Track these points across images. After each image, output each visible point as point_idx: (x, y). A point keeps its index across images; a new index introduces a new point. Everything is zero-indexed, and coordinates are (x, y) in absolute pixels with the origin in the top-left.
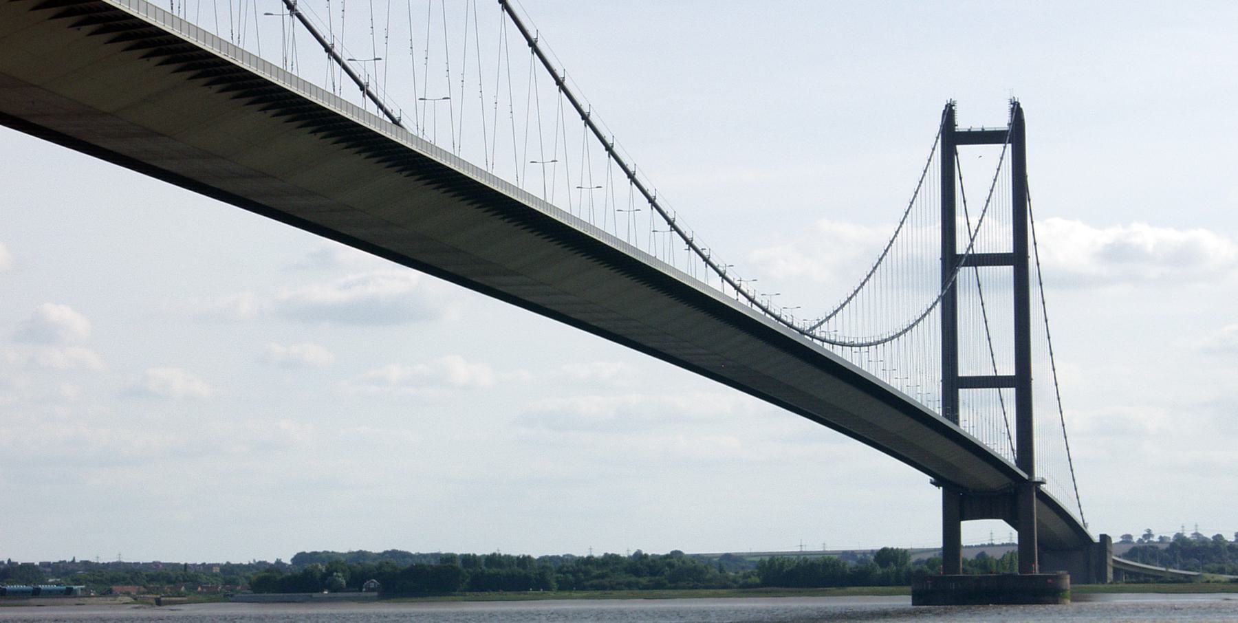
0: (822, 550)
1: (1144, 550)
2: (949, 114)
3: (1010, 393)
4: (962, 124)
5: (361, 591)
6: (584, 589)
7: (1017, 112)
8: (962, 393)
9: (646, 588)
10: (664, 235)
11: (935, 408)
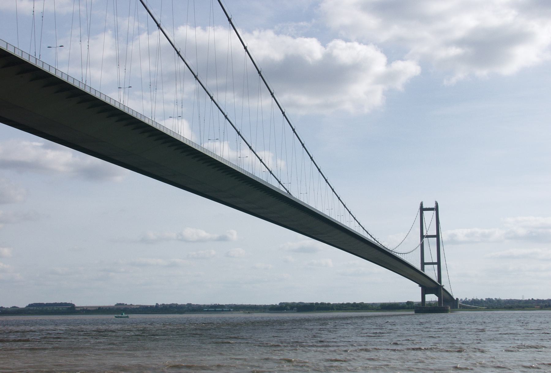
1: (466, 302)
2: (422, 204)
3: (436, 266)
4: (424, 207)
6: (342, 310)
8: (435, 234)
9: (355, 310)
10: (428, 237)
11: (418, 266)
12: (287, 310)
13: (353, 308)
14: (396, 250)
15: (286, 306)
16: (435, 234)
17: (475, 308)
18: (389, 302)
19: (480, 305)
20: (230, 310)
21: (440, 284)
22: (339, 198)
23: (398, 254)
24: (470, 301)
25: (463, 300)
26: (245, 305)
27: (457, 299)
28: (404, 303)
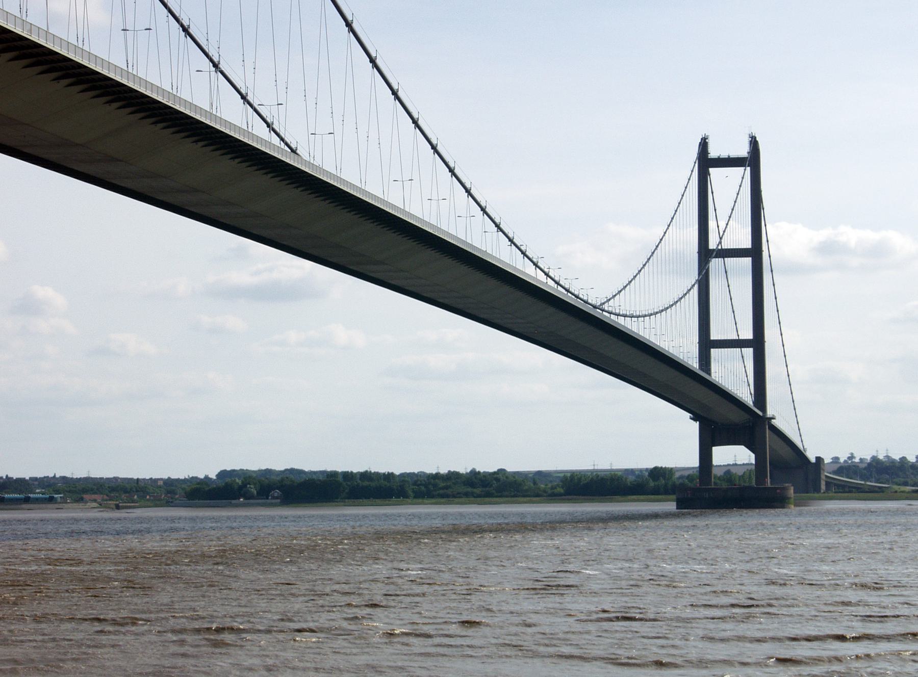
0: (609, 468)
1: (848, 468)
2: (704, 145)
3: (749, 352)
4: (713, 153)
5: (268, 499)
6: (433, 497)
7: (754, 144)
8: (714, 351)
9: (479, 496)
11: (693, 363)
12: (246, 498)
13: (470, 489)
14: (617, 304)
15: (244, 485)
16: (747, 243)
17: (876, 492)
18: (591, 468)
19: (896, 480)
20: (51, 500)
21: (760, 413)
22: (451, 171)
23: (621, 320)
24: (863, 466)
25: (842, 460)
26: (101, 479)
27: (819, 459)
28: (641, 470)
